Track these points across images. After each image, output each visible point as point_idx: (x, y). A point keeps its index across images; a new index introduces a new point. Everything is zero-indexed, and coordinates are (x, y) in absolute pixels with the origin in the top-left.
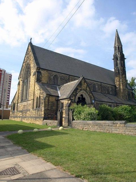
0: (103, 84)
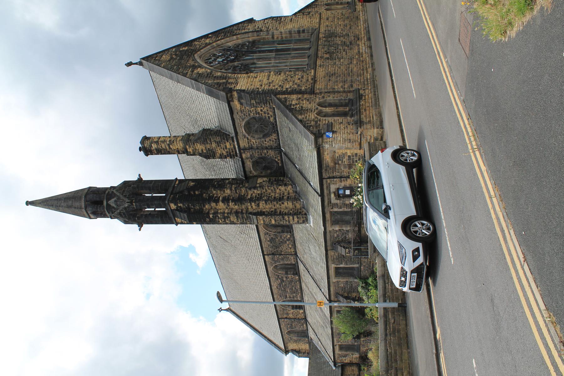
0: (264, 249)
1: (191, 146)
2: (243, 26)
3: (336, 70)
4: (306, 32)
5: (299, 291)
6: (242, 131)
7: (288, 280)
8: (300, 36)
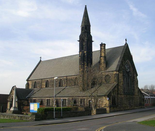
6: (107, 74)
8: (132, 90)
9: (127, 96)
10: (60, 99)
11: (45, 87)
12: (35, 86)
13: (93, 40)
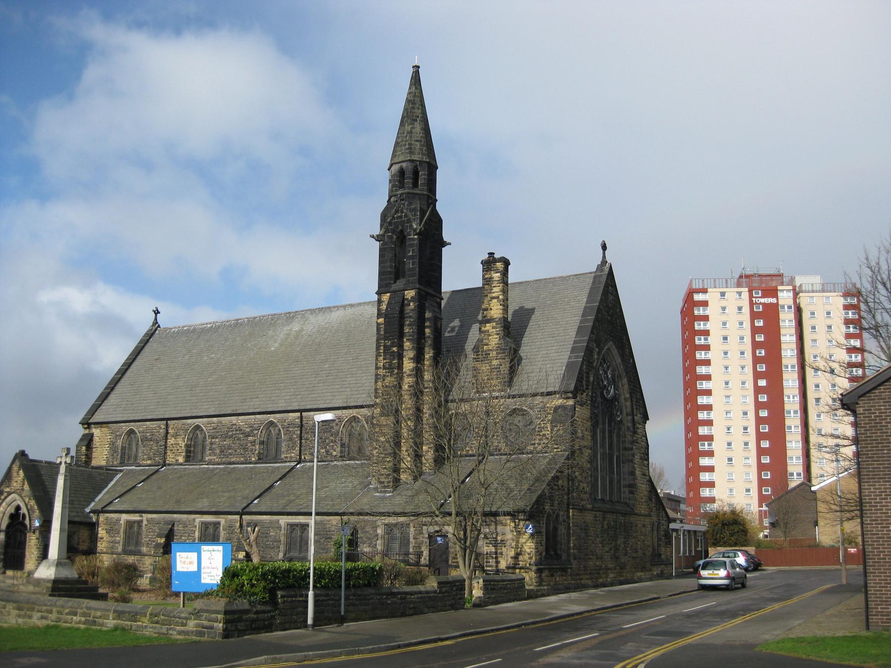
1: (494, 330)
2: (639, 406)
3: (591, 538)
4: (631, 495)
5: (224, 460)
6: (513, 404)
7: (249, 445)
8: (625, 486)
9: (604, 518)
10: (271, 522)
11: (181, 460)
12: (125, 455)
13: (446, 237)
